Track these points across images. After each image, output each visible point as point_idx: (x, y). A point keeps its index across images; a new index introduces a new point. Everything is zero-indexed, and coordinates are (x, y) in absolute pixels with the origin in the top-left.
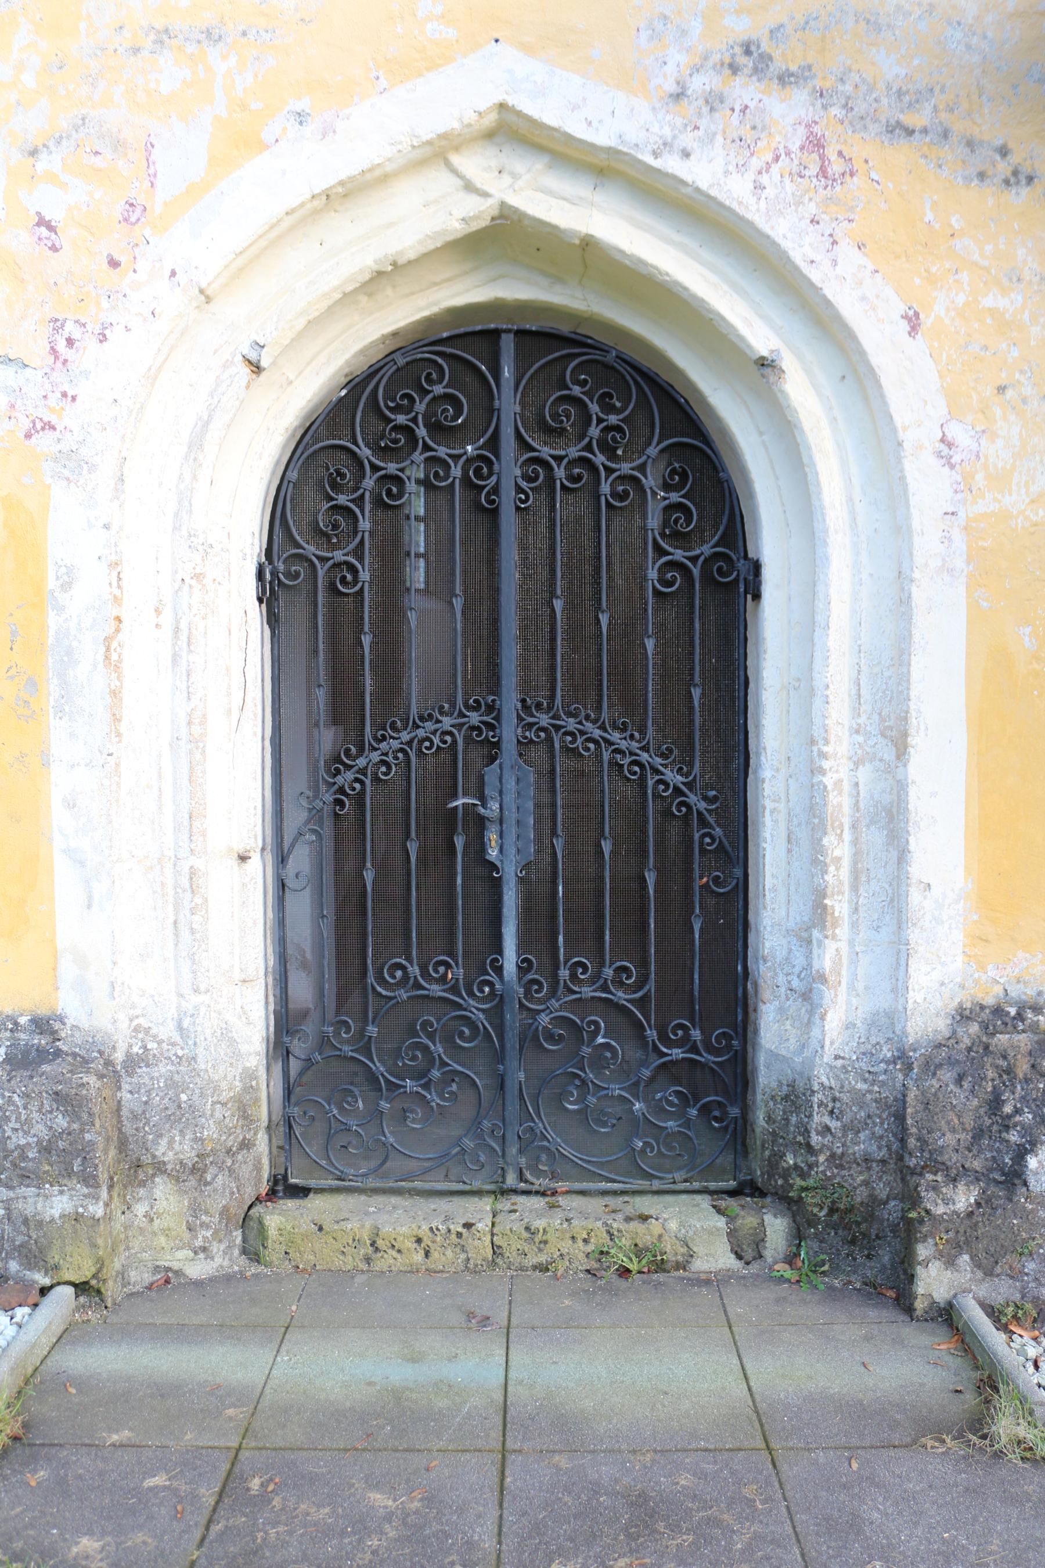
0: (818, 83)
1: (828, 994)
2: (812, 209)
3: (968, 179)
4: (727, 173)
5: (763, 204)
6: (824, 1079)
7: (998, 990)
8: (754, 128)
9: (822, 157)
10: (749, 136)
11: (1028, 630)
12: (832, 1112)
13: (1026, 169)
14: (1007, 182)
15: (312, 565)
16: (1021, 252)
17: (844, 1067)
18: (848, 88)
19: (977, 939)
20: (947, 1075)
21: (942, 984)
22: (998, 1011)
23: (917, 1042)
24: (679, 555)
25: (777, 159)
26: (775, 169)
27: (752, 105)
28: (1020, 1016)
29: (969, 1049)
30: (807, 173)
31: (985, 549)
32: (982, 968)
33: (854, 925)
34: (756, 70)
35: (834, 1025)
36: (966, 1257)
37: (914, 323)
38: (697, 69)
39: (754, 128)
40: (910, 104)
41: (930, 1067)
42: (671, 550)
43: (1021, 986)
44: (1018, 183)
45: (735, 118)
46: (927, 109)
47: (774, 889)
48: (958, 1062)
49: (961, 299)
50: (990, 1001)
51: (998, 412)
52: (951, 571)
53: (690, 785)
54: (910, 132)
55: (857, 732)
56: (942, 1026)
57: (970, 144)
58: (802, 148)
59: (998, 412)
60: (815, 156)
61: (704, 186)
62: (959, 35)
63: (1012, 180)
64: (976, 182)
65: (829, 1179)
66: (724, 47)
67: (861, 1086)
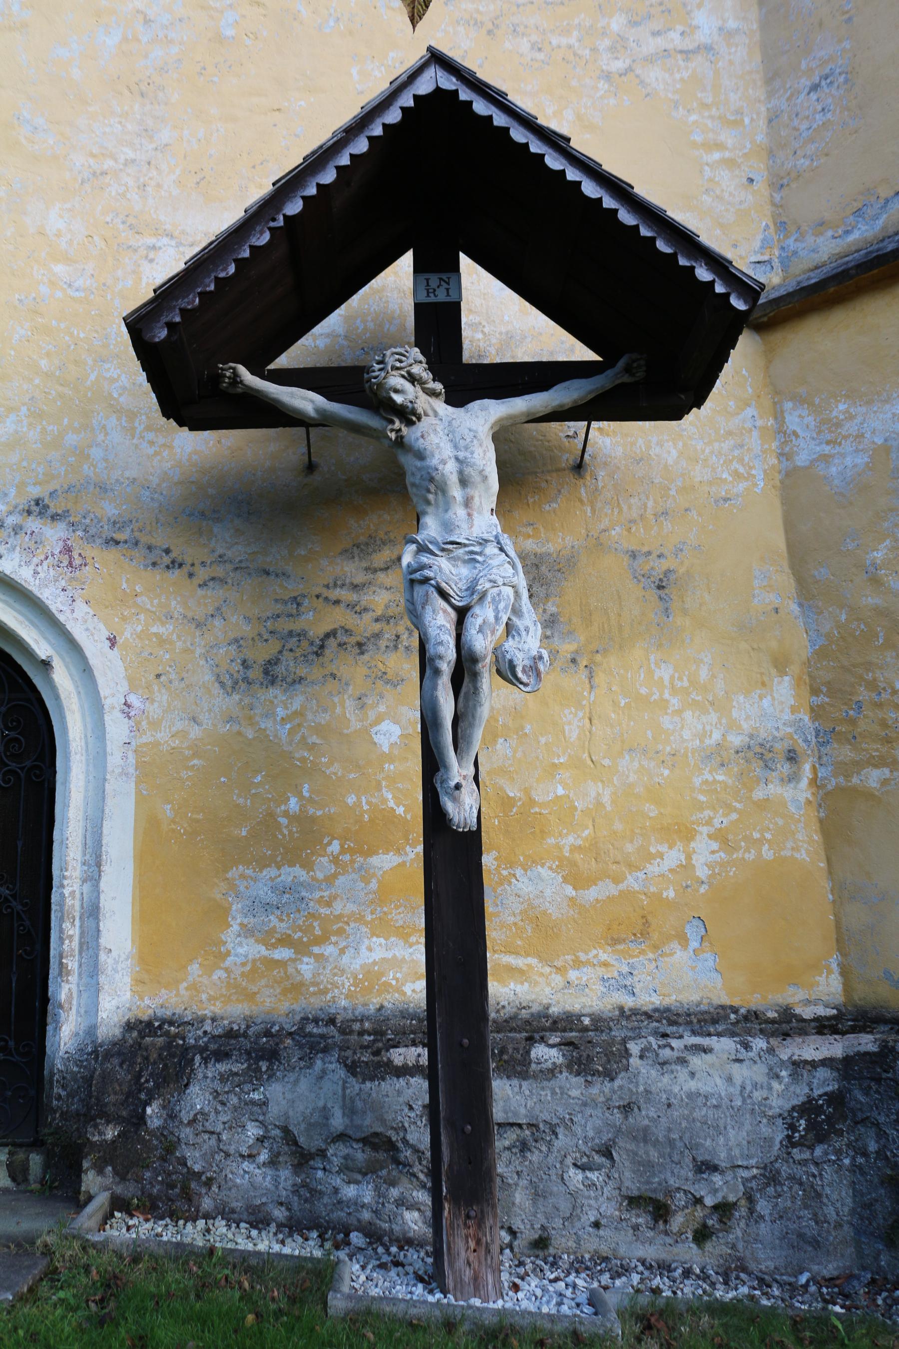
0: (72, 519)
1: (63, 1015)
2: (63, 583)
3: (146, 566)
4: (20, 566)
5: (37, 581)
6: (59, 1066)
7: (150, 1012)
8: (36, 543)
9: (70, 557)
10: (33, 547)
11: (169, 807)
12: (63, 1086)
13: (179, 560)
14: (168, 567)
15: (16, 772)
16: (173, 603)
17: (68, 1058)
18: (88, 521)
19: (138, 981)
20: (116, 1061)
21: (118, 1008)
22: (149, 1024)
23: (103, 1042)
24: (13, 766)
25: (47, 558)
26: (45, 563)
27: (36, 531)
28: (160, 1027)
29: (131, 1046)
30: (62, 565)
31: (145, 762)
32: (142, 999)
33: (80, 974)
34: (40, 513)
35: (67, 1033)
36: (110, 1168)
37: (113, 642)
38: (10, 513)
39: (36, 543)
40: (119, 528)
41: (108, 1055)
42: (10, 763)
43: (163, 1010)
44: (173, 567)
45: (27, 538)
46: (128, 530)
47: (55, 957)
48: (124, 1054)
49: (139, 629)
50: (145, 1018)
51: (156, 688)
52: (127, 774)
53: (14, 896)
54: (117, 543)
55: (84, 864)
56: (117, 1032)
57: (150, 548)
58: (60, 552)
59: (156, 688)
60: (67, 556)
61: (8, 572)
62: (147, 493)
63: (171, 566)
64: (151, 567)
65: (61, 1127)
66: (25, 502)
67: (75, 1069)
